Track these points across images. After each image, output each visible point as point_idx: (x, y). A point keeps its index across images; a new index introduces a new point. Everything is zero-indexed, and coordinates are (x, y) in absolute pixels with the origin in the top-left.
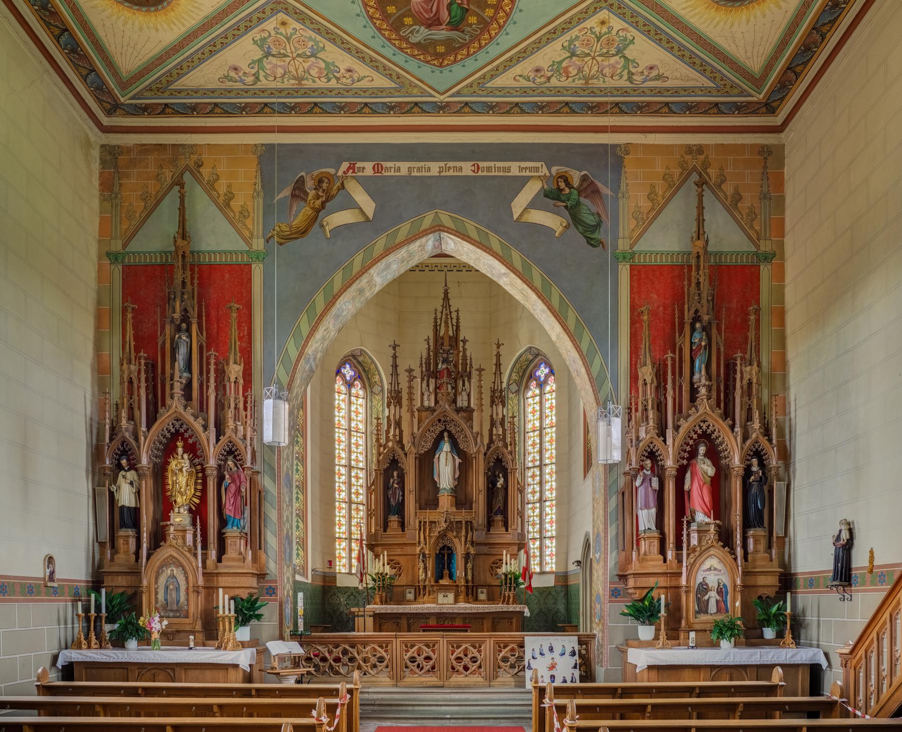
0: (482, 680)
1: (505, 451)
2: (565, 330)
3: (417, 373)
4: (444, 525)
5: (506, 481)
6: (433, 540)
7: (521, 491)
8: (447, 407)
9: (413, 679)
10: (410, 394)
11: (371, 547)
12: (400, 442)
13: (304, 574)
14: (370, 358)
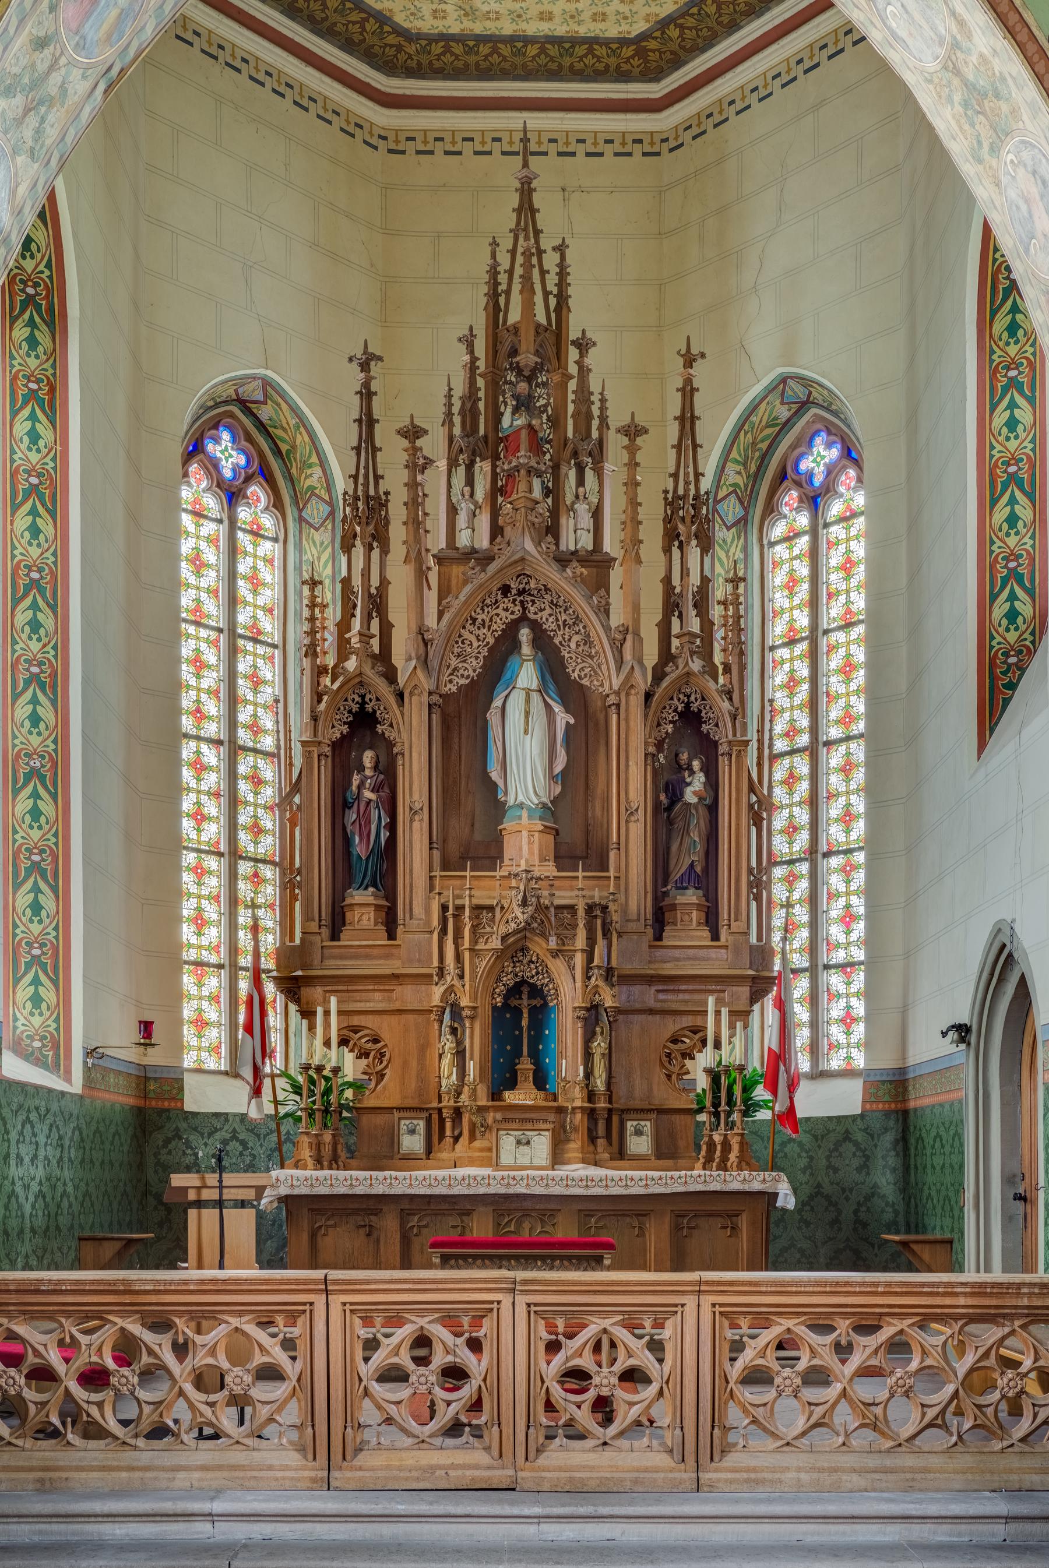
0: (662, 1460)
1: (711, 684)
2: (1010, 32)
3: (434, 445)
4: (520, 915)
5: (713, 783)
6: (483, 964)
7: (759, 813)
8: (529, 545)
9: (394, 1459)
10: (415, 503)
11: (293, 987)
12: (384, 657)
13: (59, 1065)
14: (295, 410)
